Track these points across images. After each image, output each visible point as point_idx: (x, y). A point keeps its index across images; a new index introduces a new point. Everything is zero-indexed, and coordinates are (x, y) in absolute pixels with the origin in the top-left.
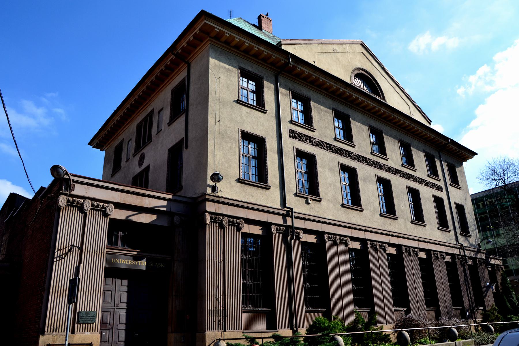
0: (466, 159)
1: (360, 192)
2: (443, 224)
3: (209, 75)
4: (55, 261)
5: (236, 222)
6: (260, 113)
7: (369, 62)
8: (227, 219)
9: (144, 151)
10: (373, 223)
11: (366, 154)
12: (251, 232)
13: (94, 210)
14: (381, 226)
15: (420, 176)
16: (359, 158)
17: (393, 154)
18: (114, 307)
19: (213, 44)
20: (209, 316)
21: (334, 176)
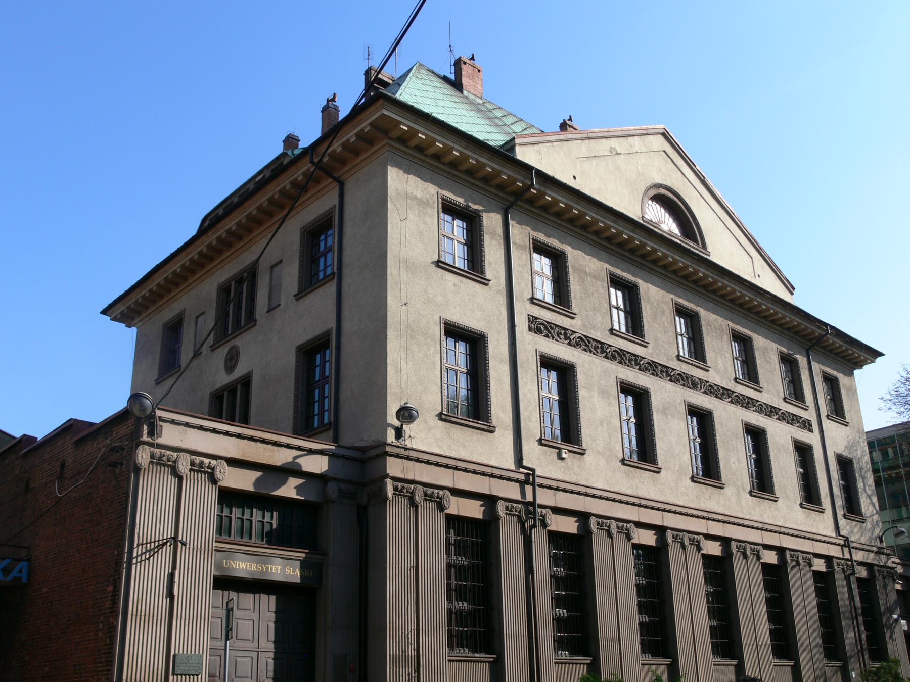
0: (859, 364)
1: (656, 436)
2: (810, 496)
3: (387, 214)
4: (134, 564)
5: (436, 495)
6: (477, 285)
7: (677, 169)
8: (421, 489)
9: (238, 342)
10: (677, 495)
11: (668, 359)
12: (461, 514)
13: (194, 471)
14: (693, 503)
15: (770, 400)
16: (653, 368)
17: (719, 357)
18: (258, 650)
19: (394, 151)
20: (392, 666)
21: (609, 405)
